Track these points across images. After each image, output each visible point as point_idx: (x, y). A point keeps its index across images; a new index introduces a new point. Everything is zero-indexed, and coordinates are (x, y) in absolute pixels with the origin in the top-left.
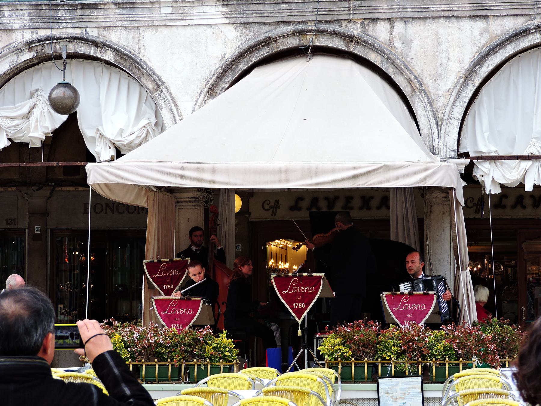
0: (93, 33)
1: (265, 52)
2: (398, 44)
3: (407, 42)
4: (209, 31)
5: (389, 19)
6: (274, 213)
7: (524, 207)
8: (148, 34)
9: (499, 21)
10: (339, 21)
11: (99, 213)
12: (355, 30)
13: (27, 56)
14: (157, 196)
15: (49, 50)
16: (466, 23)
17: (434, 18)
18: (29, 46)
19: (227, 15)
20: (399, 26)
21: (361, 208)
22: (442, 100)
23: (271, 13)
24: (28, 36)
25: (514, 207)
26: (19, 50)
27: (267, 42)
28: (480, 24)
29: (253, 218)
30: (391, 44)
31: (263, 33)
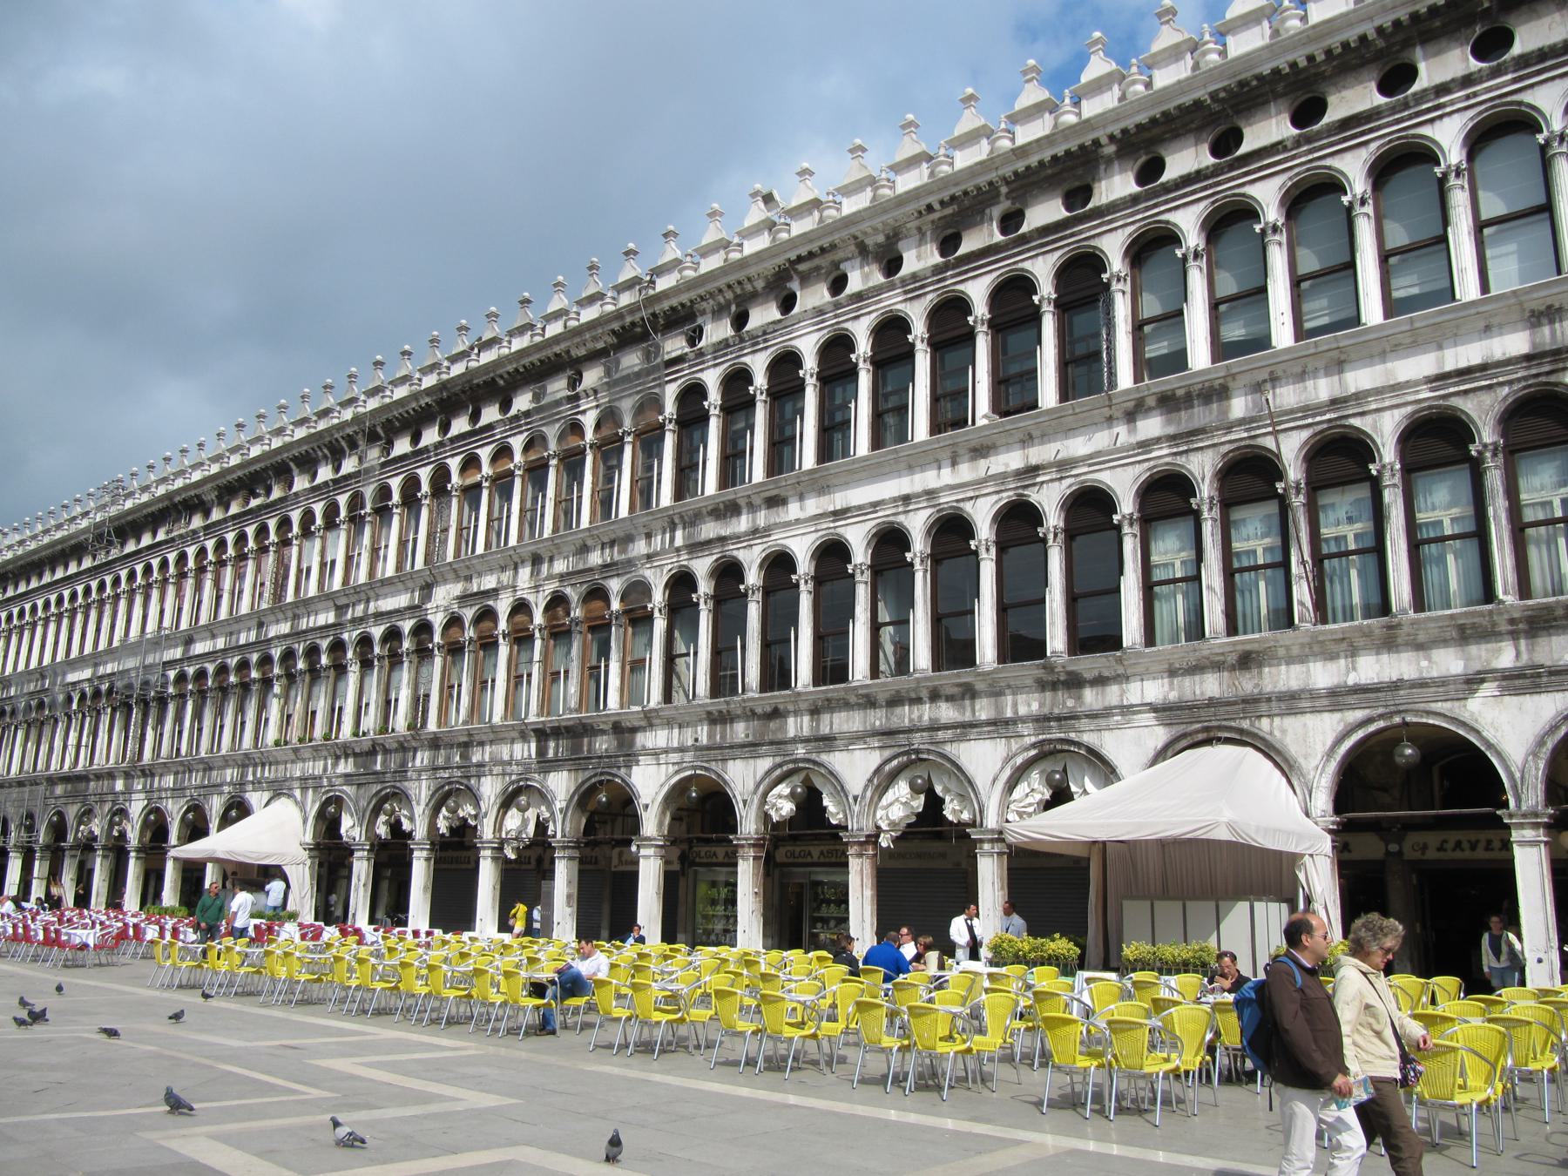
0: (1073, 735)
1: (1184, 743)
2: (1277, 733)
3: (1284, 731)
4: (1146, 730)
5: (1269, 716)
6: (1423, 854)
7: (1463, 850)
8: (1106, 734)
9: (1350, 712)
10: (1234, 719)
11: (288, 886)
12: (1245, 724)
13: (1033, 752)
14: (919, 856)
15: (1046, 748)
16: (1326, 715)
17: (1302, 713)
18: (1033, 746)
19: (1157, 718)
20: (1277, 720)
21: (1501, 849)
22: (1312, 773)
23: (261, 595)
24: (1033, 739)
25: (1454, 850)
26: (1027, 749)
27: (1184, 736)
28: (1337, 716)
29: (1406, 858)
30: (1271, 733)
31: (1181, 729)
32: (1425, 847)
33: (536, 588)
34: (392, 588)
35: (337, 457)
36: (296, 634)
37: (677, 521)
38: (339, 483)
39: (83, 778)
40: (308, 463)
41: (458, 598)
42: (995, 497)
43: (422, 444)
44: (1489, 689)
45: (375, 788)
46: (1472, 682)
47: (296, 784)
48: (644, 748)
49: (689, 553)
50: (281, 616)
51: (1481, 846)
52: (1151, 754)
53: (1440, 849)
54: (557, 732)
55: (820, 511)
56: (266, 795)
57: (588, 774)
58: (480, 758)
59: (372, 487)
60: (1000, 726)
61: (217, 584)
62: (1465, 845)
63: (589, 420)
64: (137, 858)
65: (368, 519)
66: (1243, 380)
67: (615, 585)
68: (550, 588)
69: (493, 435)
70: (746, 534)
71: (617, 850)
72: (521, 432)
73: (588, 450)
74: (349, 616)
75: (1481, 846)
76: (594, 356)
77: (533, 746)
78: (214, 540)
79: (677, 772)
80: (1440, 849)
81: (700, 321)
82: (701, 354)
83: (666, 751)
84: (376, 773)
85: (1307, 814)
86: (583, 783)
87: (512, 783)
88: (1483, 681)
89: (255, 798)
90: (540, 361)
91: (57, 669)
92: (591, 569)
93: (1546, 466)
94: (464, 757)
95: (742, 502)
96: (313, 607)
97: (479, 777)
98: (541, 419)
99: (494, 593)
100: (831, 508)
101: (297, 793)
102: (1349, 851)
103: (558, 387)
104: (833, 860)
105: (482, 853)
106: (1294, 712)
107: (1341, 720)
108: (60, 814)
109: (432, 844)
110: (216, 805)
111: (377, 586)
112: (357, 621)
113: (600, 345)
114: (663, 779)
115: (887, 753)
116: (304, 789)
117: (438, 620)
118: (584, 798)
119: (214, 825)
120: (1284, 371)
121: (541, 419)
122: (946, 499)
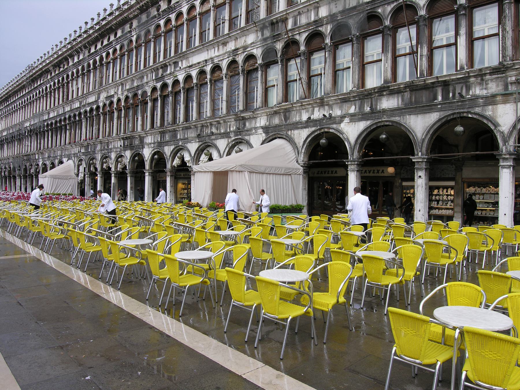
2: (292, 135)
3: (294, 135)
18: (234, 140)
24: (234, 138)
32: (314, 173)
33: (122, 94)
34: (91, 95)
35: (78, 53)
36: (71, 110)
37: (153, 71)
38: (79, 62)
39: (29, 155)
40: (72, 56)
41: (105, 98)
42: (228, 59)
43: (80, 59)
44: (347, 120)
45: (89, 156)
46: (343, 117)
47: (73, 156)
48: (146, 143)
49: (271, 40)
50: (67, 105)
51: (372, 172)
52: (261, 142)
53: (318, 173)
54: (127, 138)
55: (186, 66)
56: (67, 159)
57: (134, 151)
58: (298, 119)
59: (86, 63)
60: (226, 135)
61: (95, 76)
62: (368, 172)
63: (134, 39)
64: (131, 176)
65: (86, 74)
66: (291, 15)
67: (140, 92)
68: (126, 93)
69: (112, 45)
70: (169, 74)
71: (158, 174)
72: (119, 44)
73: (134, 49)
74: (168, 72)
75: (372, 172)
76: (135, 17)
77: (122, 141)
78: (105, 53)
79: (153, 150)
80: (318, 173)
81: (160, 3)
82: (69, 67)
83: (151, 144)
84: (89, 152)
85: (297, 162)
86: (133, 154)
87: (118, 154)
88: (345, 117)
89: (65, 160)
90: (122, 20)
91: (22, 123)
92: (134, 88)
93: (348, 47)
94: (108, 147)
95: (168, 64)
96: (74, 102)
97: (111, 153)
98: (123, 39)
99: (113, 96)
100: (189, 65)
101: (73, 158)
102: (384, 173)
103: (127, 27)
104: (186, 177)
105: (146, 174)
106: (297, 128)
107: (309, 131)
108: (26, 166)
109: (102, 173)
110: (57, 162)
111: (89, 94)
112: (84, 106)
113: (136, 13)
114: (150, 152)
115: (201, 143)
116: (74, 157)
117: (101, 105)
118: (133, 157)
119: (49, 169)
120: (302, 11)
121: (123, 39)
122: (216, 61)
